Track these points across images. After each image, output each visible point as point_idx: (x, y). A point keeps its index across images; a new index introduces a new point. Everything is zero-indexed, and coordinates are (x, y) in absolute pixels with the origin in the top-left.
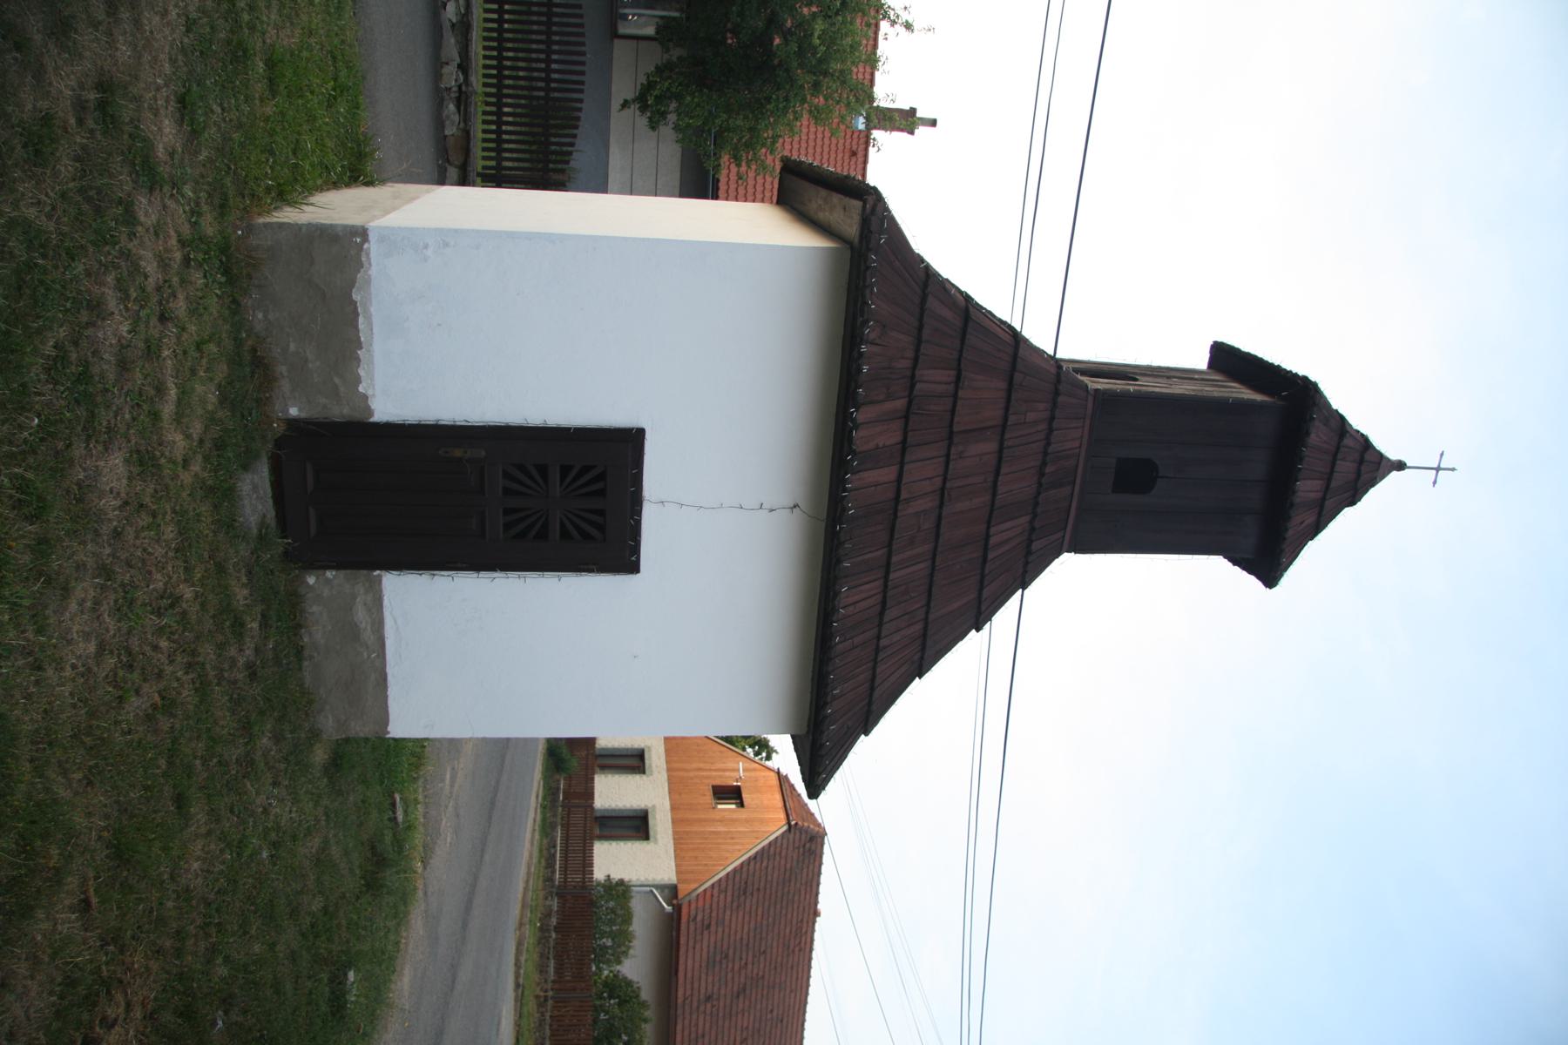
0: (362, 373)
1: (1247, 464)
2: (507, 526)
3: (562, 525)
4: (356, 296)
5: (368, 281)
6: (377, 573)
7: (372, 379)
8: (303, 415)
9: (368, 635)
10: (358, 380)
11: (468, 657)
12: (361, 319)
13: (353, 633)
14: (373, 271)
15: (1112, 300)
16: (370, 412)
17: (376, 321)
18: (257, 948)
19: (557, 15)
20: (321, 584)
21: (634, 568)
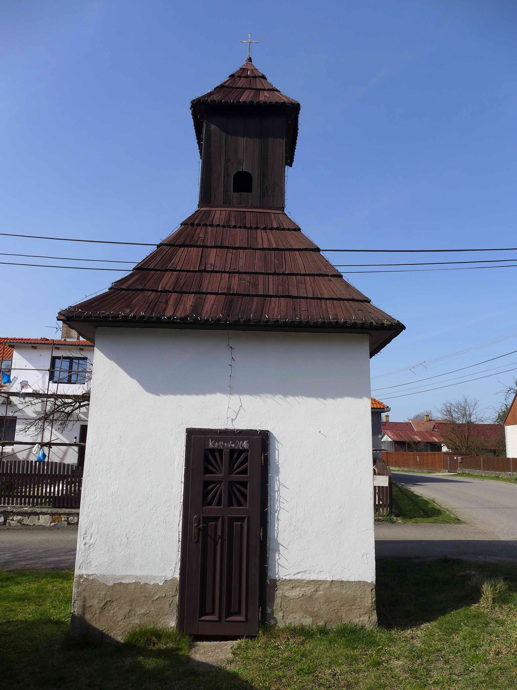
0: (152, 583)
1: (246, 131)
2: (240, 504)
3: (236, 474)
4: (111, 584)
5: (103, 576)
6: (268, 581)
7: (156, 577)
8: (175, 618)
9: (309, 590)
10: (156, 585)
11: (325, 532)
12: (124, 581)
13: (309, 598)
14: (98, 573)
15: (163, 193)
16: (173, 580)
17: (124, 573)
18: (286, 654)
19: (60, 472)
20: (286, 615)
21: (187, 429)
